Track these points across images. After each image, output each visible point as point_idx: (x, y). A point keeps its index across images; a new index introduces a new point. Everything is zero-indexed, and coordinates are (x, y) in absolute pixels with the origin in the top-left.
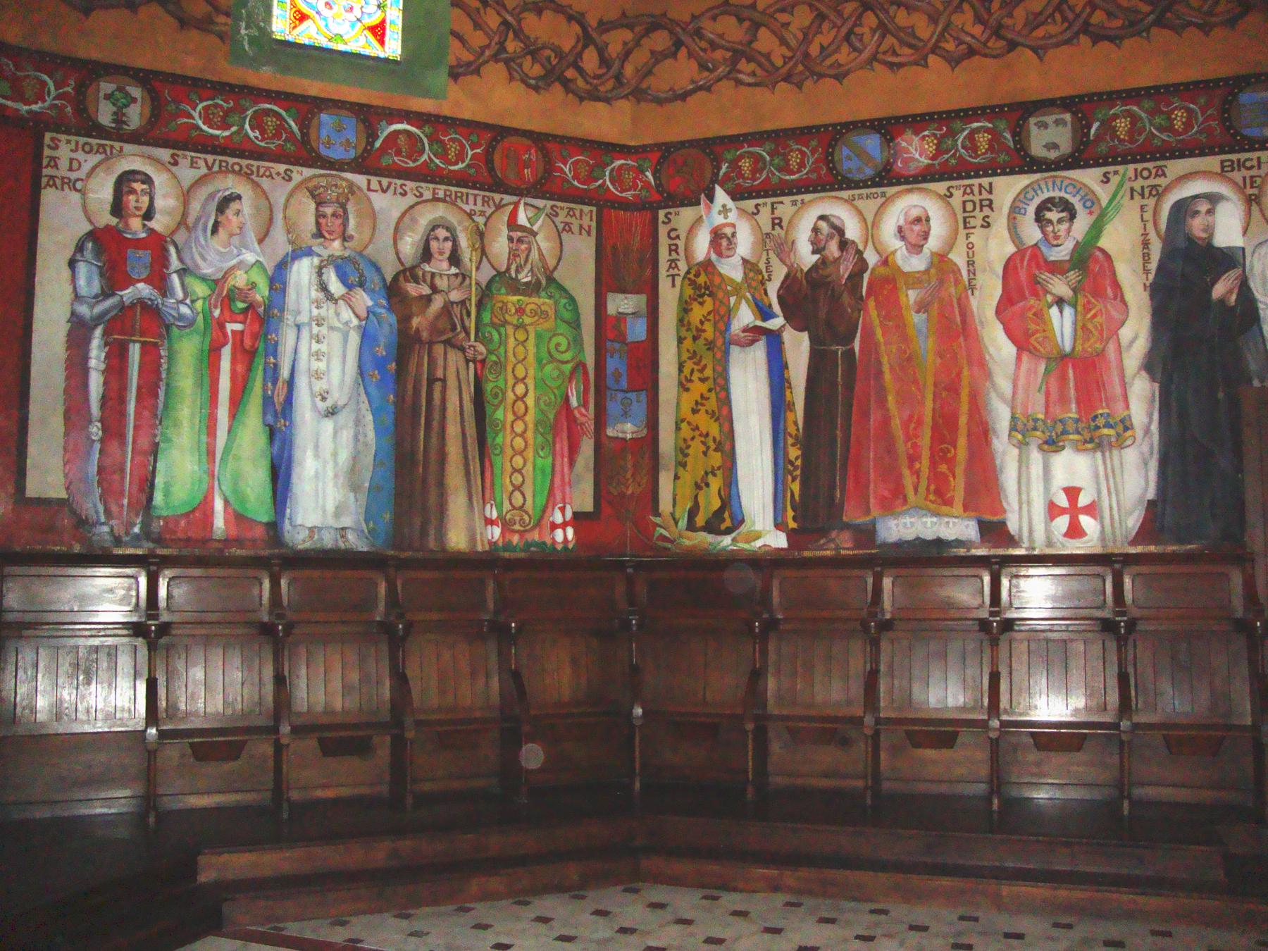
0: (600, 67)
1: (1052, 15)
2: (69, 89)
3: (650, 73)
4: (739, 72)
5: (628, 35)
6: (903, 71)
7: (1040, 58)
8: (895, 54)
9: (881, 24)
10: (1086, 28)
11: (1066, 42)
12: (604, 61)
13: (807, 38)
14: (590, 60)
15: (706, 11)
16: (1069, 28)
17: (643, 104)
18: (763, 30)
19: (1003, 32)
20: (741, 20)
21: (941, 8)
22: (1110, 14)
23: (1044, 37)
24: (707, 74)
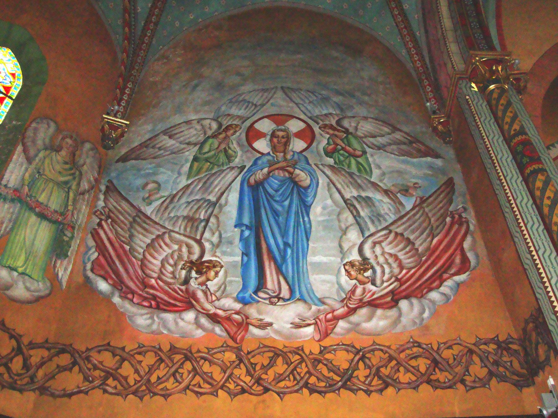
0: (23, 368)
1: (289, 376)
2: (500, 68)
3: (53, 377)
4: (107, 385)
5: (46, 353)
6: (203, 397)
7: (282, 399)
8: (200, 387)
9: (194, 369)
10: (306, 385)
11: (297, 391)
12: (26, 366)
13: (151, 371)
14: (17, 364)
15: (96, 347)
16: (297, 384)
17: (44, 397)
18: (126, 363)
19: (262, 382)
20: (114, 355)
21: (229, 365)
22: (318, 379)
23: (284, 388)
24: (87, 383)
